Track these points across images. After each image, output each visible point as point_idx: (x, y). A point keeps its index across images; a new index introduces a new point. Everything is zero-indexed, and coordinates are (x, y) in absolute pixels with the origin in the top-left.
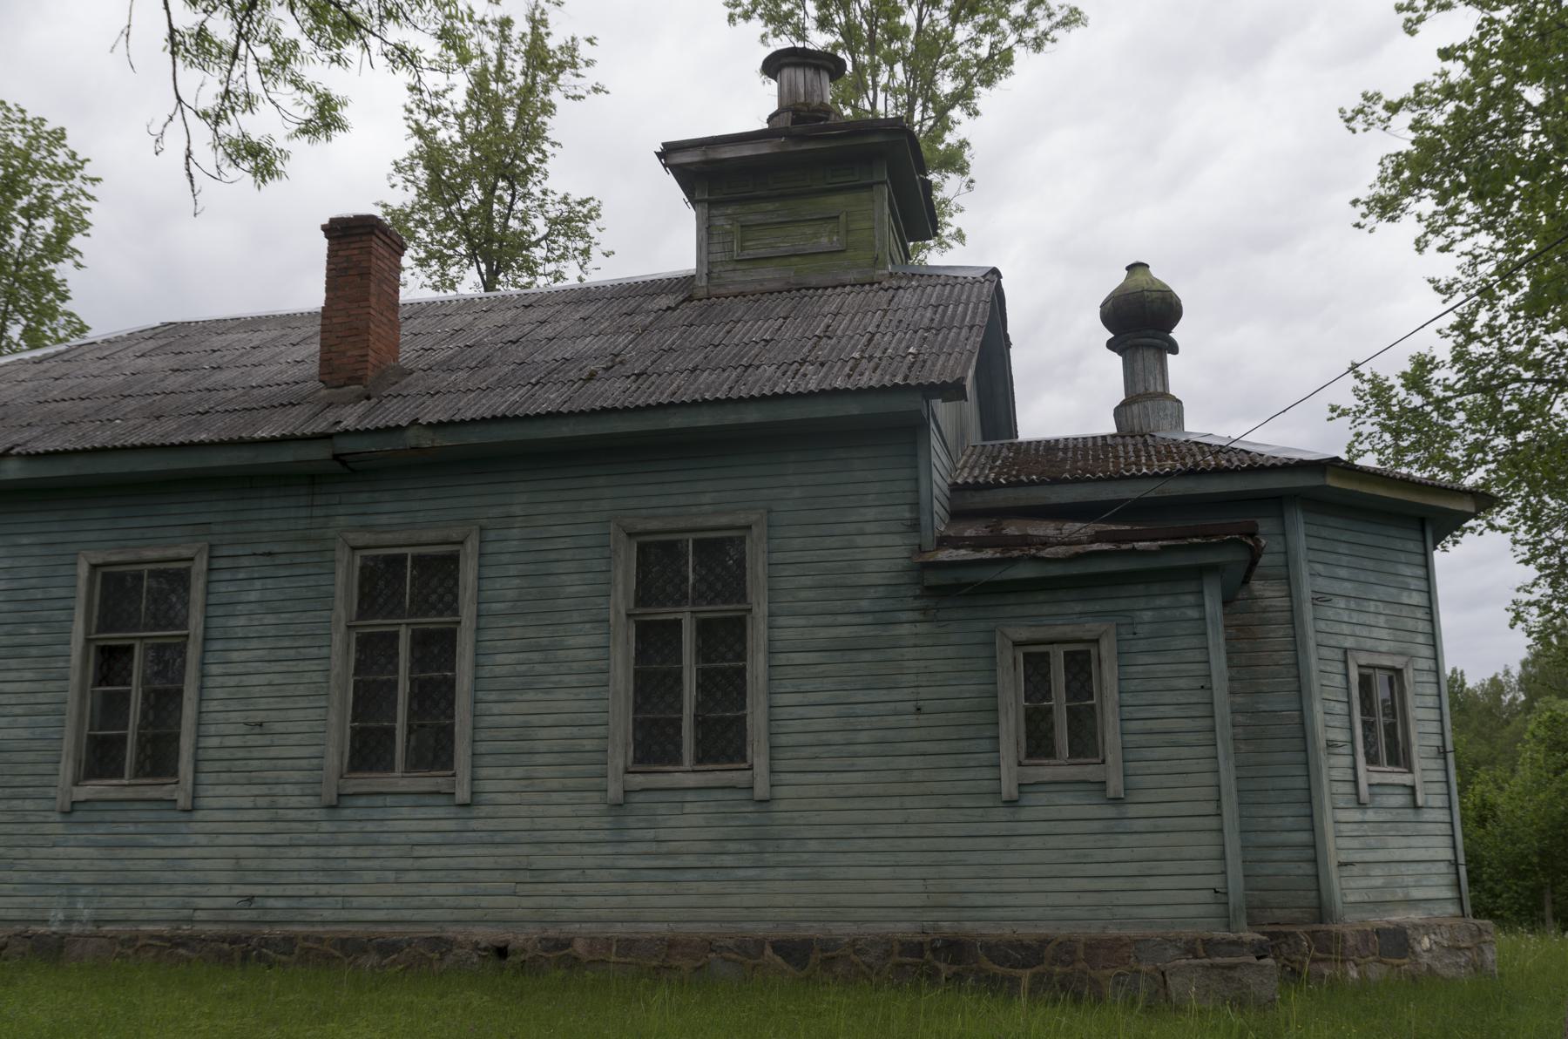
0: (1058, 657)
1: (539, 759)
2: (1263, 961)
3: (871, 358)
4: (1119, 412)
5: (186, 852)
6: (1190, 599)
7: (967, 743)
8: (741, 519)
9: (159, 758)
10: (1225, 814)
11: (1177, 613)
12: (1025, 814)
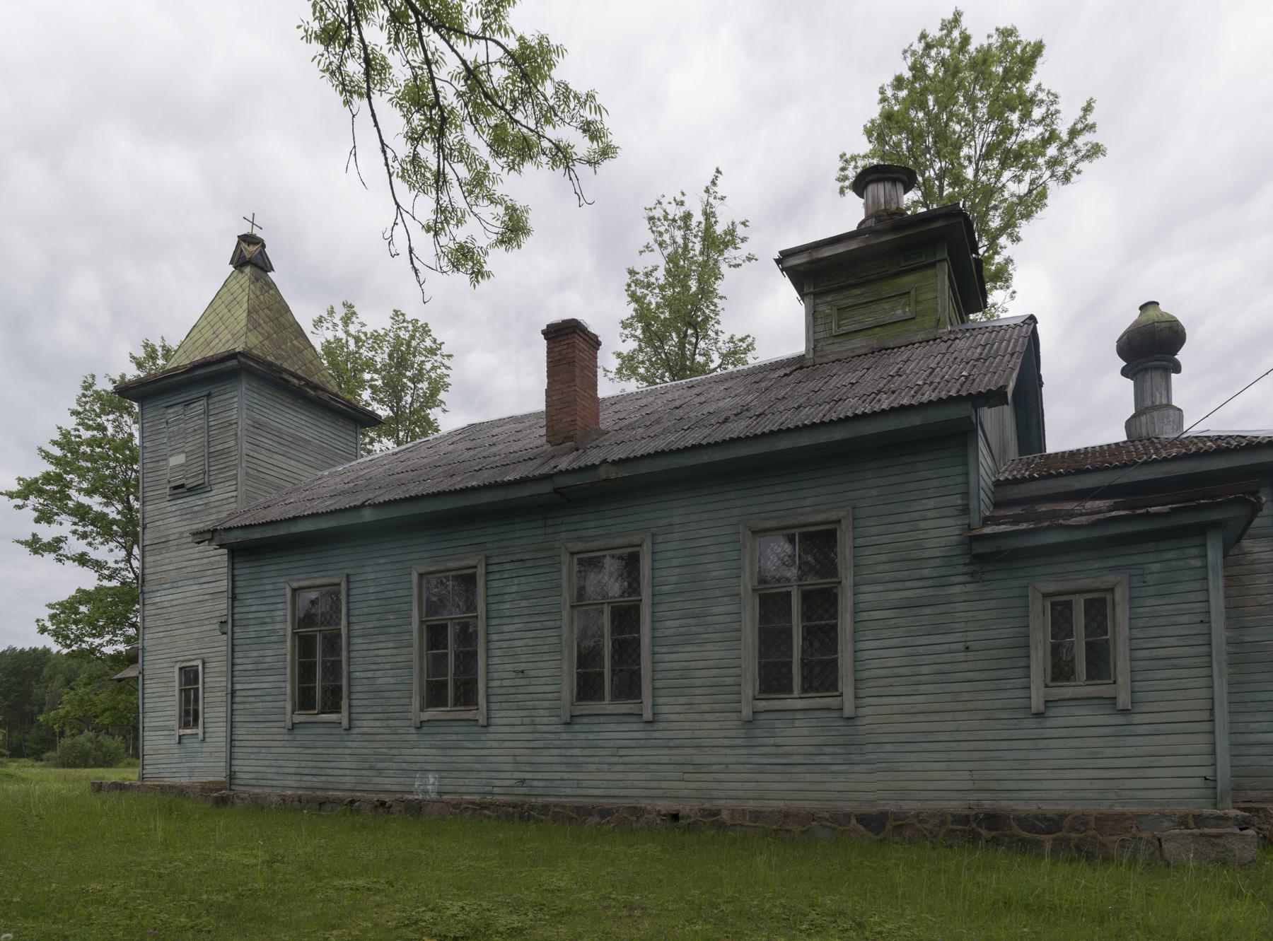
0: (1079, 604)
1: (696, 691)
2: (1245, 832)
3: (932, 383)
4: (1129, 425)
5: (486, 752)
6: (1195, 551)
7: (1004, 672)
8: (833, 515)
9: (466, 695)
10: (1217, 720)
11: (1182, 563)
12: (1049, 723)
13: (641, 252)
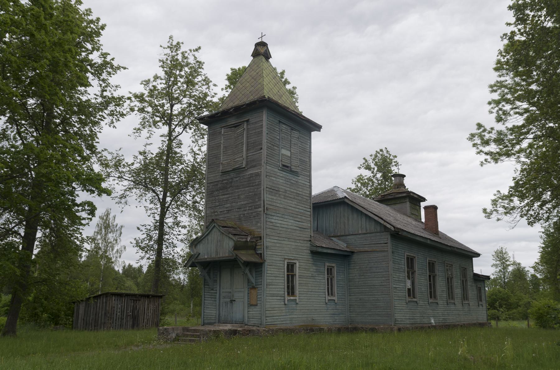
13: (161, 46)
